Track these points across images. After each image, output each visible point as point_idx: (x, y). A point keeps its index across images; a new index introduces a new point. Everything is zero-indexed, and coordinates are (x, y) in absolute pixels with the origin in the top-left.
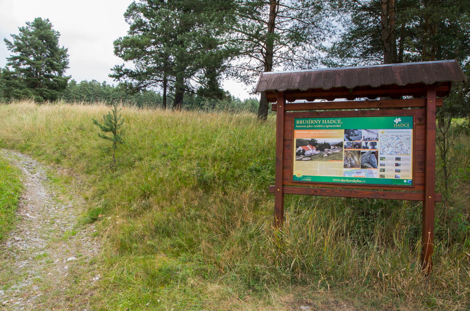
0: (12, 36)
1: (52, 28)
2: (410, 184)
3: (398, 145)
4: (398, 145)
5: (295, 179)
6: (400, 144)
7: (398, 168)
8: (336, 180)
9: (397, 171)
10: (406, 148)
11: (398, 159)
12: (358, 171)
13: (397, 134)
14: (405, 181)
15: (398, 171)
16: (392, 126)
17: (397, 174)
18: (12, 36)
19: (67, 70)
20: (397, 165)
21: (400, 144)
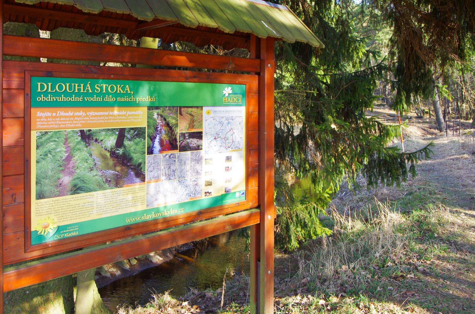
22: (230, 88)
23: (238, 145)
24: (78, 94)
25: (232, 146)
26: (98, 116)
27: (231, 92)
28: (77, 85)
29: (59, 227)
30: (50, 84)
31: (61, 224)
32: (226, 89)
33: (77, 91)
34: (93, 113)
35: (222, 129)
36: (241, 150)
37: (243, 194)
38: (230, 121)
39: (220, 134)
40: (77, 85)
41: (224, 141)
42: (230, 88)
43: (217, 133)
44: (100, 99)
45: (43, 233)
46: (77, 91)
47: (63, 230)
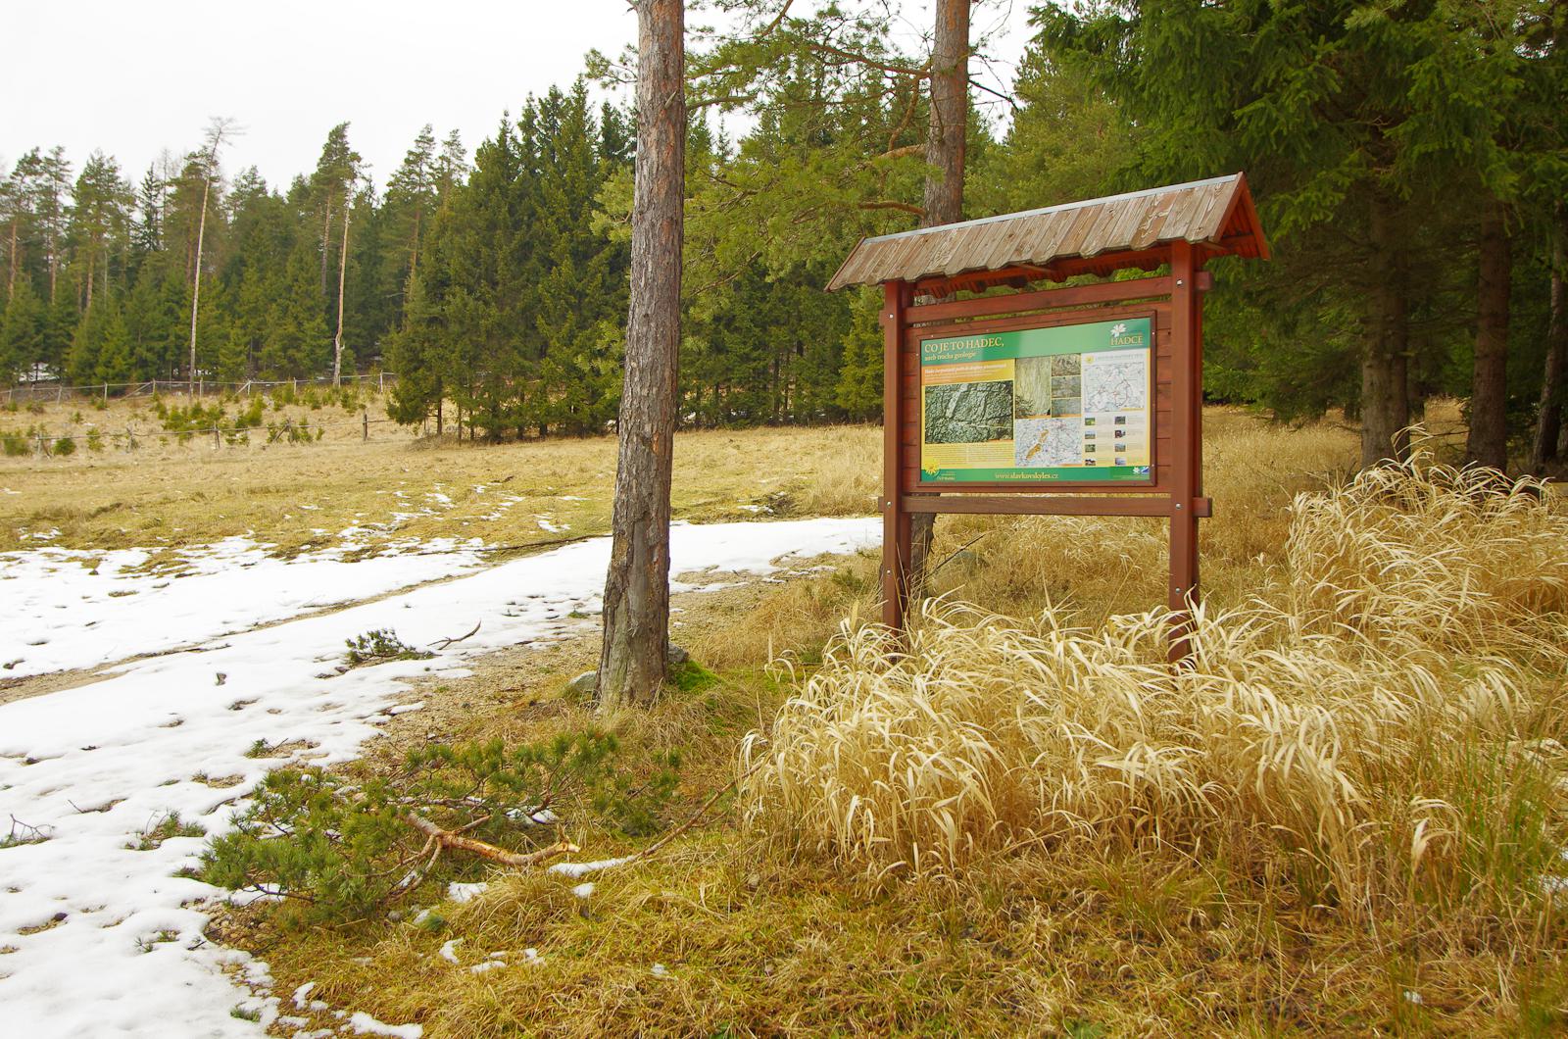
0: (184, 904)
1: (132, 174)
2: (1146, 477)
3: (1120, 388)
4: (1120, 388)
5: (925, 481)
6: (1125, 385)
7: (1120, 441)
8: (1018, 477)
9: (1120, 449)
10: (1136, 393)
11: (1120, 420)
12: (156, 667)
13: (1118, 362)
14: (1136, 470)
15: (1120, 449)
16: (1108, 345)
17: (1119, 454)
18: (184, 904)
19: (122, 175)
20: (1119, 434)
21: (1125, 385)
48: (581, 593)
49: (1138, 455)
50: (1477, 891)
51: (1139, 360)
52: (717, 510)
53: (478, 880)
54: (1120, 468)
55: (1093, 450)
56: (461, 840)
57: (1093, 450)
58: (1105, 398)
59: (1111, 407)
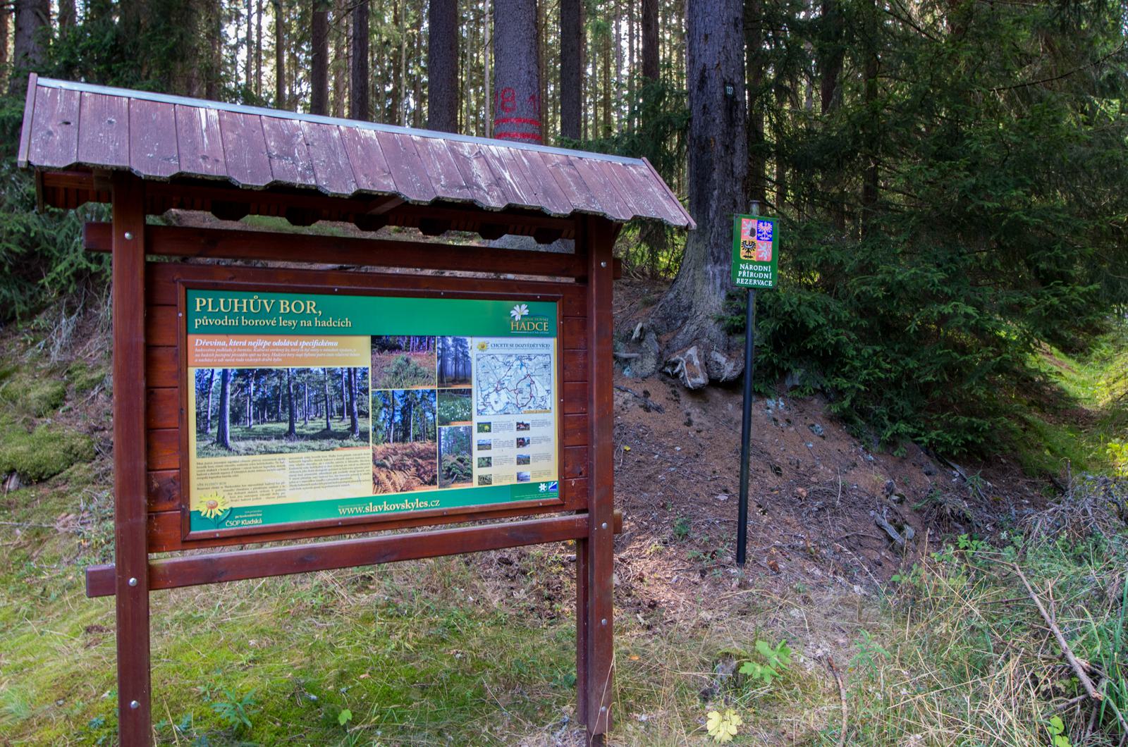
2: (555, 497)
3: (523, 385)
4: (523, 385)
6: (528, 381)
7: (524, 451)
8: (377, 508)
9: (523, 460)
10: (542, 393)
13: (521, 352)
14: (543, 487)
15: (523, 460)
16: (504, 329)
20: (521, 443)
21: (528, 381)
22: (524, 306)
23: (542, 403)
24: (231, 315)
25: (531, 404)
26: (213, 347)
27: (526, 312)
28: (236, 301)
29: (232, 509)
30: (210, 300)
31: (235, 505)
32: (517, 308)
33: (236, 310)
34: (261, 343)
35: (509, 374)
36: (549, 412)
37: (554, 487)
38: (527, 361)
39: (506, 383)
40: (236, 301)
41: (514, 395)
42: (524, 306)
43: (499, 382)
44: (235, 322)
45: (208, 516)
46: (236, 310)
47: (238, 514)
48: (222, 460)
49: (545, 470)
50: (1084, 615)
51: (544, 351)
52: (272, 405)
53: (1061, 389)
54: (525, 486)
55: (489, 464)
56: (425, 741)
57: (489, 464)
58: (504, 396)
59: (511, 408)
